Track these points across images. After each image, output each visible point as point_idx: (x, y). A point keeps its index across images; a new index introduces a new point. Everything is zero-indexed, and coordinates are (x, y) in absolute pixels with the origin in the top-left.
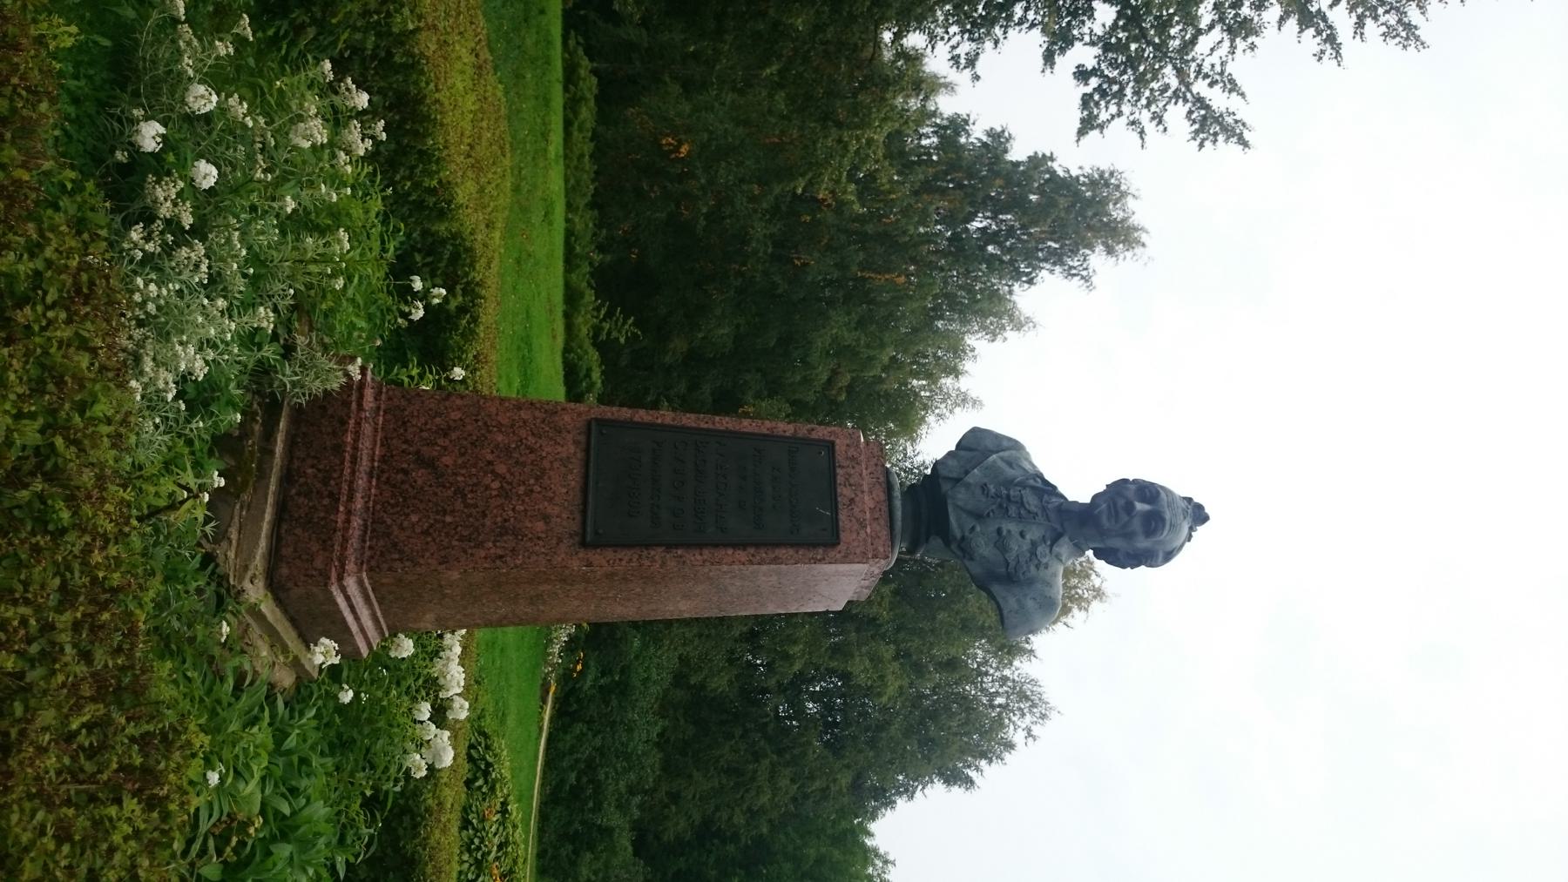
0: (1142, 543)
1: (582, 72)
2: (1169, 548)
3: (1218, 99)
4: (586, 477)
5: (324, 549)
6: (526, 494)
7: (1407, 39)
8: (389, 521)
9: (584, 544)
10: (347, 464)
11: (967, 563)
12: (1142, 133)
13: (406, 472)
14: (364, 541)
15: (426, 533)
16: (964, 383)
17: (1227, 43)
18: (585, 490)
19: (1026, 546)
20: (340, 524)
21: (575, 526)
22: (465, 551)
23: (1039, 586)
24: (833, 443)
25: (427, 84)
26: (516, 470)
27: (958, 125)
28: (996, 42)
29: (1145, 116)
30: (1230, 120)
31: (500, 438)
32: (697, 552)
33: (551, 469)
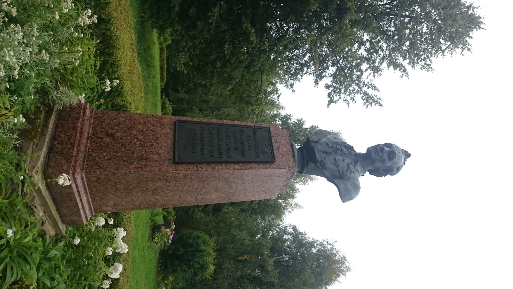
0: (389, 164)
1: (167, 105)
2: (398, 167)
3: (371, 92)
4: (175, 139)
5: (68, 163)
6: (150, 146)
7: (428, 69)
8: (94, 155)
9: (174, 163)
10: (78, 134)
11: (324, 171)
12: (348, 103)
13: (102, 138)
14: (84, 162)
15: (110, 159)
16: (296, 201)
17: (372, 75)
18: (174, 144)
19: (345, 165)
20: (74, 154)
21: (171, 157)
22: (125, 166)
23: (352, 180)
24: (269, 128)
25: (114, 29)
26: (146, 138)
27: (287, 117)
28: (299, 80)
29: (348, 98)
30: (375, 98)
31: (140, 127)
32: (220, 166)
33: (161, 137)
